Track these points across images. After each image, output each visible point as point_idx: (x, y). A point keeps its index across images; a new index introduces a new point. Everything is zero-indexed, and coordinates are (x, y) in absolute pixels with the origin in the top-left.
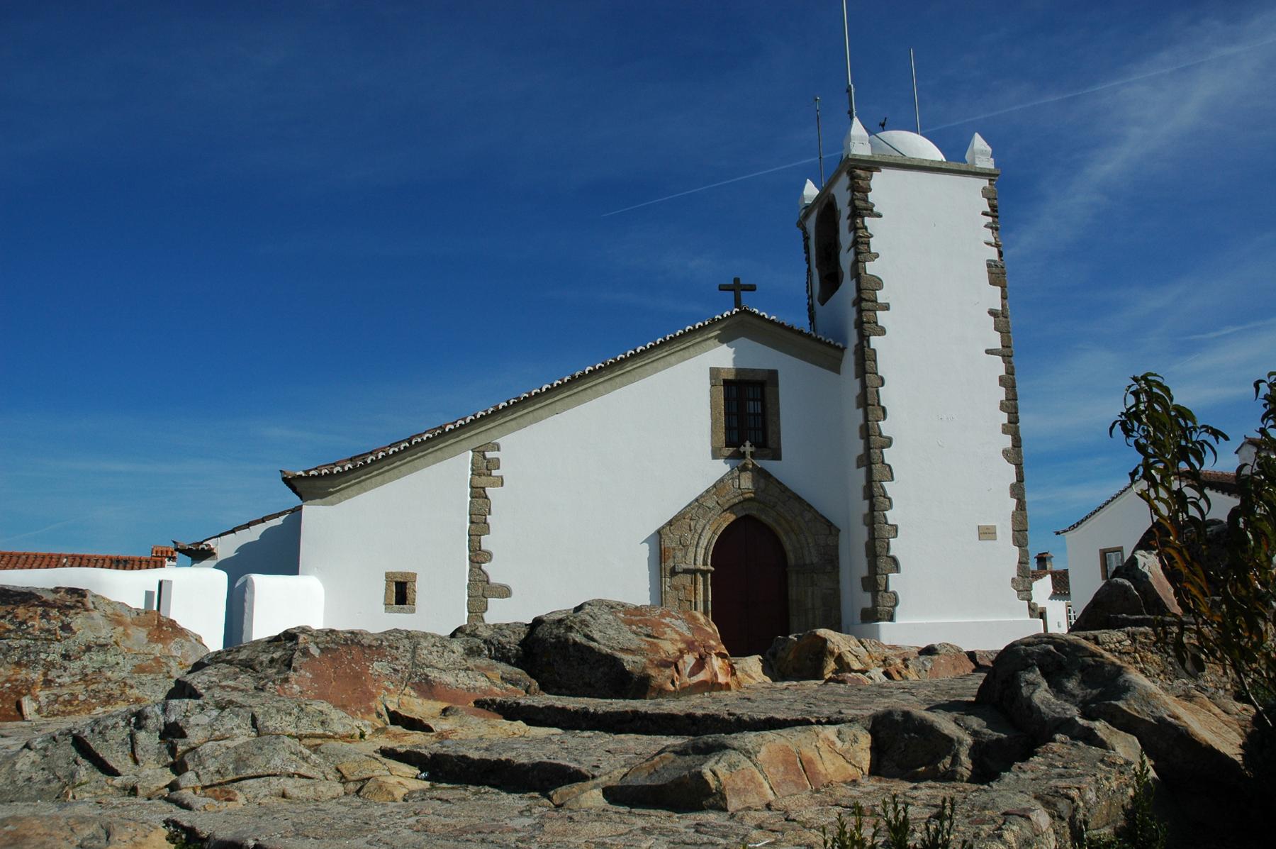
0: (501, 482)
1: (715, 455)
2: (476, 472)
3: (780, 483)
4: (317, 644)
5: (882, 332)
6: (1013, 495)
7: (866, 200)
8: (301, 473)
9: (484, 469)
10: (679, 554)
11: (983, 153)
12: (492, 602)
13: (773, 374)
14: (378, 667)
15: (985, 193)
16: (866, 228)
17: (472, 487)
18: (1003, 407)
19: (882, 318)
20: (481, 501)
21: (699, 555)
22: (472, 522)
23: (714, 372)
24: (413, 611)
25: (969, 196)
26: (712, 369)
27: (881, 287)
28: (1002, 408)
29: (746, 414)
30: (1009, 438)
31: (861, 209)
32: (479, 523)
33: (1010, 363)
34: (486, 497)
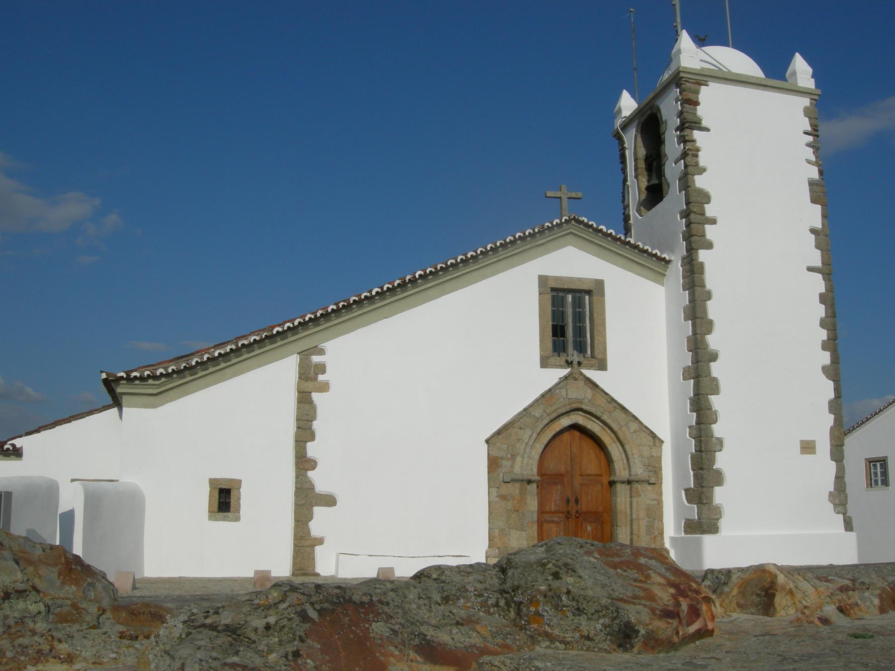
0: (324, 387)
1: (544, 363)
3: (606, 394)
4: (312, 604)
5: (709, 246)
6: (831, 411)
8: (123, 374)
9: (310, 378)
12: (318, 511)
13: (600, 284)
14: (379, 628)
15: (807, 112)
18: (823, 324)
19: (710, 232)
20: (307, 407)
21: (527, 464)
23: (543, 280)
24: (238, 519)
27: (708, 202)
30: (827, 355)
31: (689, 123)
32: (305, 431)
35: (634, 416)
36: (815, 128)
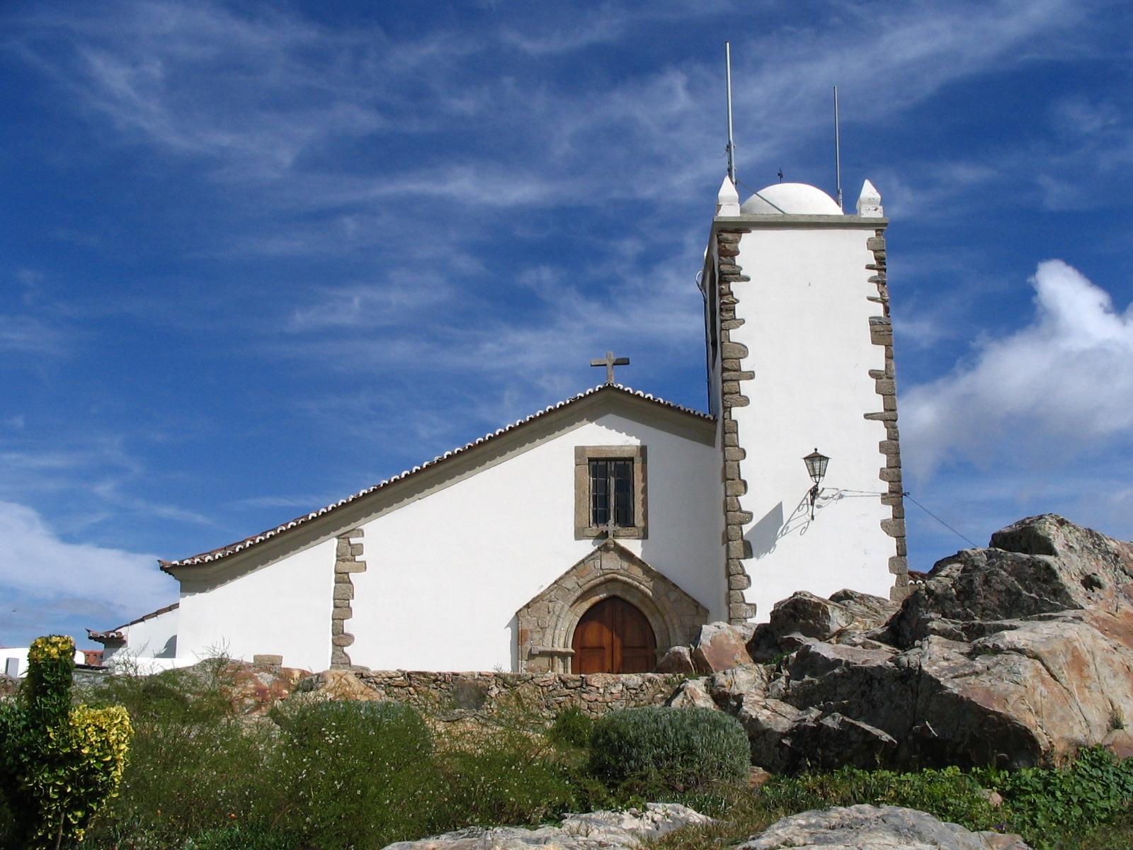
0: (363, 567)
1: (579, 534)
2: (340, 558)
5: (745, 401)
6: (892, 570)
7: (733, 265)
8: (176, 562)
9: (349, 558)
10: (536, 636)
11: (870, 201)
15: (870, 244)
16: (732, 293)
17: (336, 573)
18: (883, 475)
19: (746, 387)
20: (344, 586)
22: (335, 607)
23: (580, 451)
25: (855, 250)
26: (576, 448)
28: (882, 477)
29: (610, 492)
32: (342, 607)
33: (894, 427)
34: (350, 582)
35: (674, 585)
36: (880, 260)
